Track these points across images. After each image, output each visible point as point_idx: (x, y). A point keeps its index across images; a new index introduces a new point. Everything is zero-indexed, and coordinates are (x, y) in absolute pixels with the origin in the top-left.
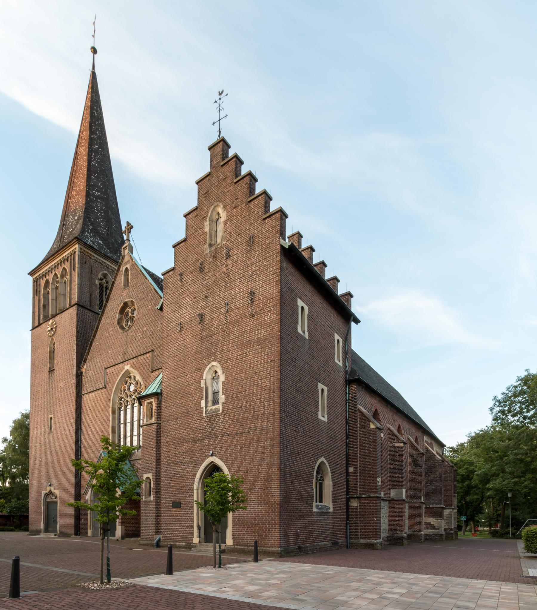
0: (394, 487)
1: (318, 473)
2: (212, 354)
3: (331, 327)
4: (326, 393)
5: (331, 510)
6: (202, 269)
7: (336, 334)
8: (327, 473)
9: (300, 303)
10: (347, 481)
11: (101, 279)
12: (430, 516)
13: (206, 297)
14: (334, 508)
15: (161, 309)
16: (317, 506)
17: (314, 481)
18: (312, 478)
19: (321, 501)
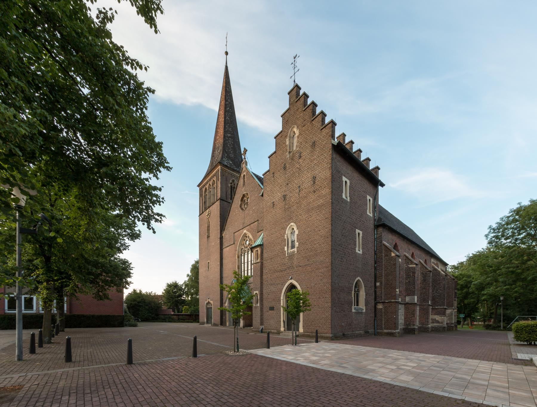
0: (408, 295)
1: (355, 287)
2: (291, 218)
3: (364, 192)
4: (361, 235)
5: (364, 311)
6: (285, 168)
7: (368, 196)
8: (362, 287)
9: (344, 179)
10: (375, 292)
11: (231, 183)
12: (435, 314)
13: (287, 184)
14: (366, 309)
15: (262, 195)
16: (355, 308)
17: (353, 292)
18: (352, 291)
19: (357, 305)
